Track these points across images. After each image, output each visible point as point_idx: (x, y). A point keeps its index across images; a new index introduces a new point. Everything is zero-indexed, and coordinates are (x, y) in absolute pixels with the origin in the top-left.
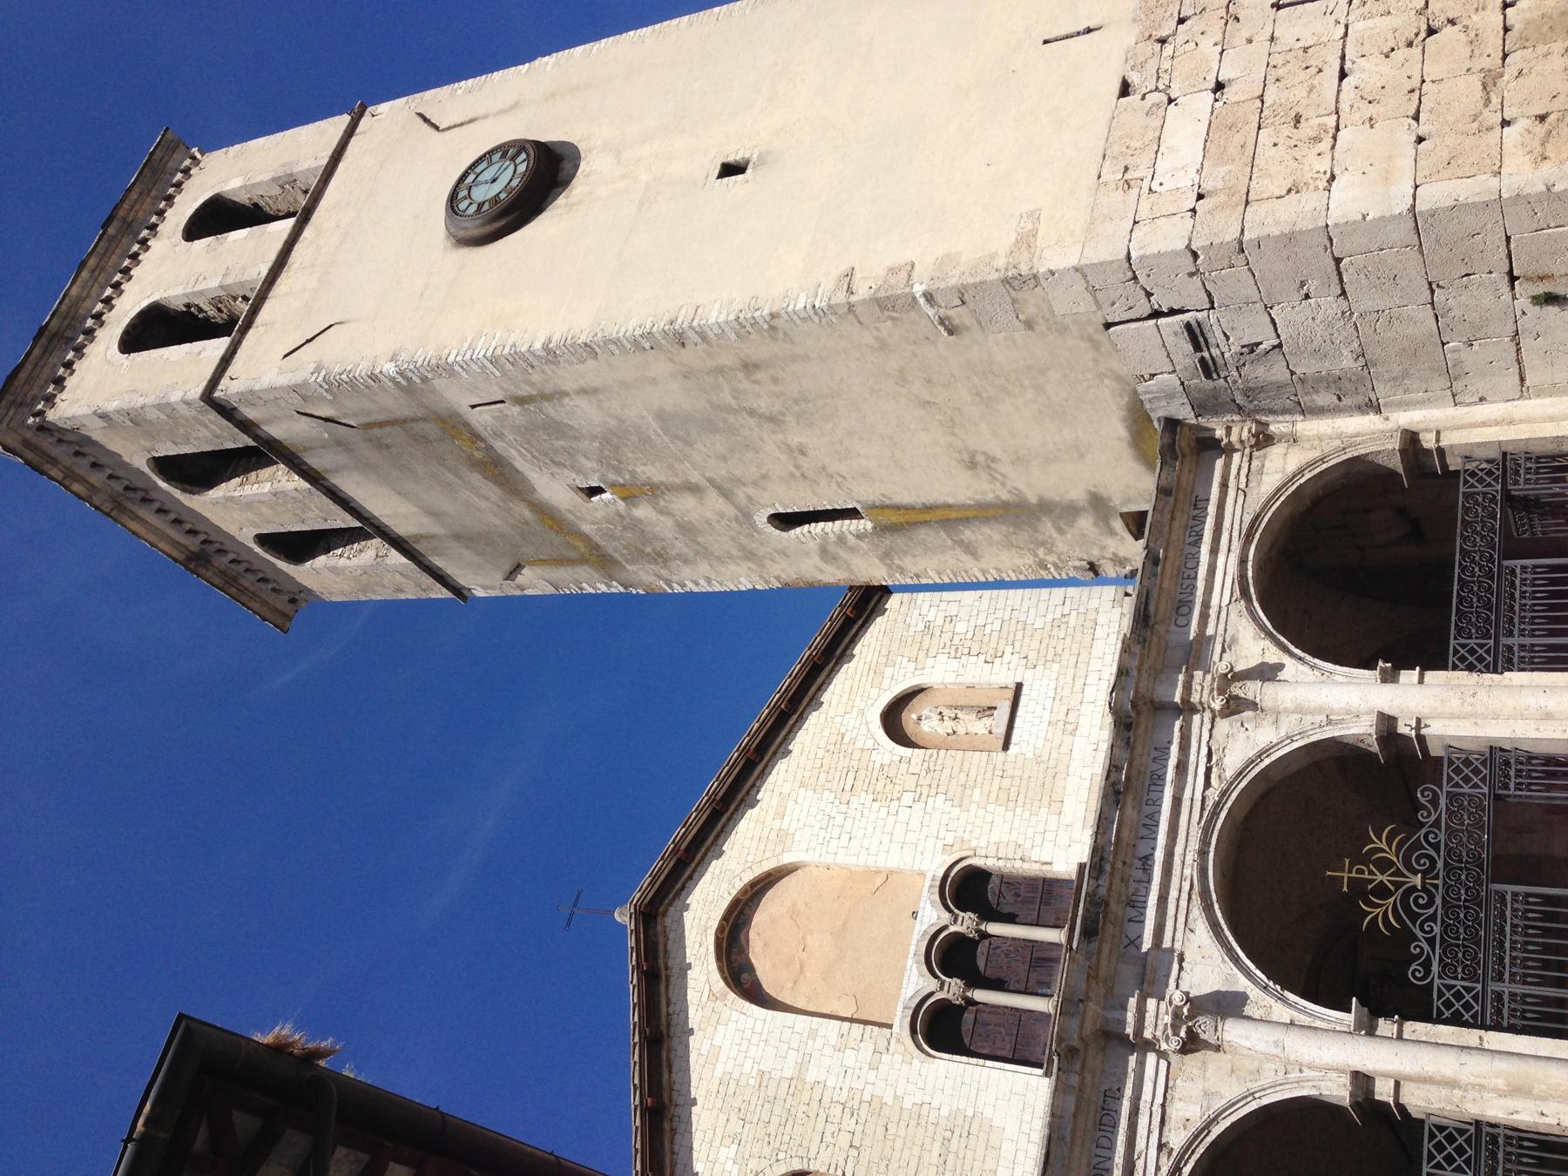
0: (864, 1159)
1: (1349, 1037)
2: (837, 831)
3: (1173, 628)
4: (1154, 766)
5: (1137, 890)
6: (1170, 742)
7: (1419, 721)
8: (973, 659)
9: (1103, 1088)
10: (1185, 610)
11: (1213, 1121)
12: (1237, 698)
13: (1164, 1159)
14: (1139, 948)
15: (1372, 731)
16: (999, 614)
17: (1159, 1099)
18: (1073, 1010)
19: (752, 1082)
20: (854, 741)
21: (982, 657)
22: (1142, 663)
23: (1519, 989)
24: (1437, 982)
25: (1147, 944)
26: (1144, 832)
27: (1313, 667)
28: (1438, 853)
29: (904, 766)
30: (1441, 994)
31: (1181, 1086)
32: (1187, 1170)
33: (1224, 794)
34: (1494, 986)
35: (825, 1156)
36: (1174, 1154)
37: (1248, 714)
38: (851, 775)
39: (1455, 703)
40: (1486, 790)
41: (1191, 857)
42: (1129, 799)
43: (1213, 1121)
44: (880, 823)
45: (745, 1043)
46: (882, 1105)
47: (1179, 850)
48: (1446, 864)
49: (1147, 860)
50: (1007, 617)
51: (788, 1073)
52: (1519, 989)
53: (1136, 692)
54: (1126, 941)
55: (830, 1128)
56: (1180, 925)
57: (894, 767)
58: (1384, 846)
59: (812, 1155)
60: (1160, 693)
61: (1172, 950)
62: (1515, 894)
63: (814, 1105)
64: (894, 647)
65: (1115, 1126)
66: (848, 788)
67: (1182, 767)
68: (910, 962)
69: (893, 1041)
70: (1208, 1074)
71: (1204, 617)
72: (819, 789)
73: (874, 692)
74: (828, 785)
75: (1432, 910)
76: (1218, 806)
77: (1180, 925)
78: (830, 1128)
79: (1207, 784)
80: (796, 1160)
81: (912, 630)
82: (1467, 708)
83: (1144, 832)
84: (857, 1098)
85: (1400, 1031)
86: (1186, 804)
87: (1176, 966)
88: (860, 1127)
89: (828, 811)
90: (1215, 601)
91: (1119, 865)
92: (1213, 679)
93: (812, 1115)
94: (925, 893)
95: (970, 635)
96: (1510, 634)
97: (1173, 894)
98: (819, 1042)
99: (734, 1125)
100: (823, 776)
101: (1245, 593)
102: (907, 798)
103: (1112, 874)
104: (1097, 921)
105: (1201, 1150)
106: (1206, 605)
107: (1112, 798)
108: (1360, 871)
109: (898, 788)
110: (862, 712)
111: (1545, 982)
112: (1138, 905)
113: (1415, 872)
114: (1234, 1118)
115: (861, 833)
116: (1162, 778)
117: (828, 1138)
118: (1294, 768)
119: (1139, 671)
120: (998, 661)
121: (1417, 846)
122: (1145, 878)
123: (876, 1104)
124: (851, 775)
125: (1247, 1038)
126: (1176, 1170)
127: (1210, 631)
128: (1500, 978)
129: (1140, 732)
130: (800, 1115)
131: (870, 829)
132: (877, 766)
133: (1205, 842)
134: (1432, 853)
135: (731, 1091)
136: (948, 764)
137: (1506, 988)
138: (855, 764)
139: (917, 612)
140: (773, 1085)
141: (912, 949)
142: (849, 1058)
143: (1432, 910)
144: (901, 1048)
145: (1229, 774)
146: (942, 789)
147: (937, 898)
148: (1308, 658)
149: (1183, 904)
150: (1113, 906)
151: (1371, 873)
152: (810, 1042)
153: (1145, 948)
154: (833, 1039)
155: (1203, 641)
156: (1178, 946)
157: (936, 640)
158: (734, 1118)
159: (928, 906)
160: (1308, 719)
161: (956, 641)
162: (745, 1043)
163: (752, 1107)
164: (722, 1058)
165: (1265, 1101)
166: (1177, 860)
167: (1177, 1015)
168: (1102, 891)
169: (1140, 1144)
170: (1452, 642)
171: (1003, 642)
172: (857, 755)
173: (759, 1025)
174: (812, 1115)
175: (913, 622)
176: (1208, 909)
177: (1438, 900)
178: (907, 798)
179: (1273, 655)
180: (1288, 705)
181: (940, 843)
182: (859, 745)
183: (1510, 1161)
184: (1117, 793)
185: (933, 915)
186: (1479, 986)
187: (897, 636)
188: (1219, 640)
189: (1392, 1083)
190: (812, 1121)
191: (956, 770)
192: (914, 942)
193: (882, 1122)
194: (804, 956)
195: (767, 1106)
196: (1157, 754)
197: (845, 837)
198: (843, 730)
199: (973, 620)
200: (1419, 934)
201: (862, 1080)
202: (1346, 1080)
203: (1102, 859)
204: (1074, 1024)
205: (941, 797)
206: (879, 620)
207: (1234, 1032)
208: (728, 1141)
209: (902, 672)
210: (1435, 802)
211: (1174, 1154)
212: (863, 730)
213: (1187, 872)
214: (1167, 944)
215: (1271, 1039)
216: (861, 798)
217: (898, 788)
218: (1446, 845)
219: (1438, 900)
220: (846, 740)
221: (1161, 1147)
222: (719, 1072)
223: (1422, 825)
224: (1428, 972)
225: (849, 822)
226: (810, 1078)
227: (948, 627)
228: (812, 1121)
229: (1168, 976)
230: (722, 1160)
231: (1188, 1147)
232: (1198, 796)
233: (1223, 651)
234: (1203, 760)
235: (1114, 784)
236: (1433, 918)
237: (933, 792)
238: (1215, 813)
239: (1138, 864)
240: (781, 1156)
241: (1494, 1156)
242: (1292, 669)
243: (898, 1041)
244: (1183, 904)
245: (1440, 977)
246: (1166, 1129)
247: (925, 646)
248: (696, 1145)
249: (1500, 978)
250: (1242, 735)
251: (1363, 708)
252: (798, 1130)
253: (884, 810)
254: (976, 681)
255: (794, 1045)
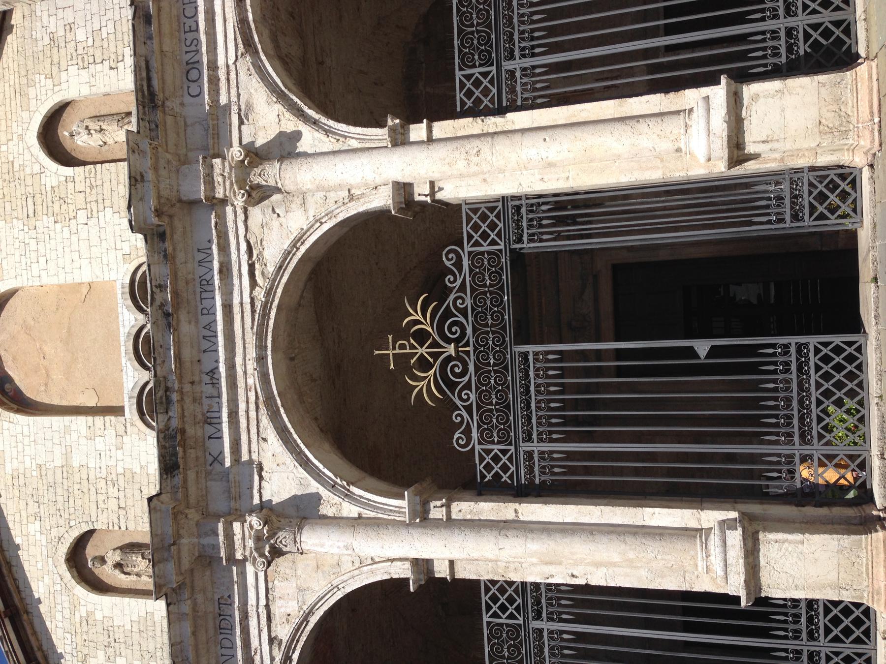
0: (131, 516)
1: (404, 531)
2: (34, 255)
3: (188, 99)
4: (202, 271)
5: (210, 406)
6: (210, 241)
7: (432, 184)
8: (99, 67)
9: (216, 597)
10: (194, 74)
11: (310, 612)
12: (259, 186)
13: (276, 651)
14: (222, 464)
15: (390, 202)
16: (110, 14)
17: (263, 602)
18: (166, 555)
19: (34, 473)
20: (23, 167)
21: (106, 63)
22: (157, 159)
23: (547, 447)
24: (478, 448)
25: (228, 463)
26: (205, 345)
27: (328, 132)
28: (466, 318)
29: (71, 185)
30: (482, 459)
31: (280, 587)
32: (295, 656)
33: (270, 292)
34: (525, 447)
35: (103, 518)
36: (284, 645)
37: (276, 197)
38: (30, 200)
39: (461, 165)
40: (502, 247)
41: (251, 365)
42: (183, 316)
43: (310, 612)
44: (67, 243)
45: (20, 445)
46: (133, 474)
47: (239, 360)
48: (475, 330)
49: (213, 372)
50: (117, 18)
51: (58, 463)
52: (547, 447)
53: (159, 197)
54: (211, 459)
55: (101, 498)
56: (254, 437)
57: (62, 188)
58: (419, 317)
59: (94, 519)
60: (187, 193)
61: (251, 461)
62: (536, 354)
63: (85, 482)
64: (30, 64)
65: (232, 628)
66: (31, 215)
67: (225, 270)
68: (124, 360)
69: (128, 425)
70: (299, 572)
71: (214, 81)
72: (8, 220)
73: (25, 115)
74: (15, 214)
75: (466, 378)
76: (266, 306)
77: (254, 437)
78: (101, 498)
79: (253, 284)
80: (83, 524)
81: (40, 44)
82: (474, 169)
83: (205, 345)
84: (114, 472)
85: (449, 513)
86: (237, 309)
87: (256, 478)
88: (122, 494)
89: (21, 237)
90: (221, 62)
91: (187, 388)
92: (231, 167)
93: (85, 490)
94: (120, 301)
95: (90, 42)
96: (511, 57)
97: (242, 406)
98: (74, 435)
99: (33, 508)
100: (8, 205)
101: (249, 44)
102: (82, 216)
103: (181, 400)
104: (175, 454)
105: (304, 638)
106: (213, 66)
107: (162, 322)
108: (402, 347)
109: (72, 207)
110: (21, 137)
111: (569, 437)
112: (212, 421)
113: (448, 341)
114: (326, 607)
115: (54, 256)
116: (210, 283)
117: (101, 505)
118: (334, 239)
119: (156, 169)
120: (121, 65)
121: (448, 314)
122: (216, 394)
123: (128, 475)
124: (30, 200)
125: (322, 546)
126: (287, 658)
127: (223, 100)
128: (529, 439)
129: (178, 236)
130: (77, 492)
131: (60, 249)
132: (49, 189)
133: (261, 346)
134: (461, 319)
135: (22, 483)
136: (106, 178)
137: (535, 447)
138: (30, 189)
139: (39, 24)
140: (50, 473)
141: (123, 349)
142: (100, 444)
143: (466, 378)
144: (135, 430)
145: (271, 269)
146: (108, 203)
147: (129, 302)
148: (323, 120)
149: (253, 414)
150: (190, 431)
151: (412, 347)
152: (67, 436)
153: (228, 463)
154: (84, 431)
155: (220, 113)
156: (255, 457)
157: (63, 51)
158: (31, 503)
159: (125, 311)
160: (332, 196)
161: (80, 51)
162: (20, 445)
163: (41, 492)
164: (8, 460)
165: (349, 590)
166: (239, 370)
167: (258, 538)
168: (175, 423)
169: (255, 643)
170: (458, 74)
171: (120, 44)
172: (29, 181)
173: (26, 429)
174: (85, 490)
175: (39, 36)
176: (274, 416)
177: (471, 367)
178: (82, 216)
179: (291, 124)
180: (309, 186)
181: (120, 254)
182: (28, 171)
183: (551, 605)
184: (167, 315)
185: (129, 319)
186: (512, 448)
187: (29, 53)
188: (234, 108)
189: (447, 563)
190: (87, 496)
191: (114, 182)
192: (123, 343)
193: (137, 486)
194: (46, 363)
195: (51, 490)
196: (201, 256)
197: (42, 260)
198: (11, 159)
199: (89, 23)
200: (458, 403)
201: (113, 459)
202: (407, 565)
203: (167, 389)
204: (170, 567)
205: (109, 211)
206: (9, 38)
207: (310, 542)
208: (32, 519)
209: (43, 90)
210: (459, 265)
211: (284, 645)
212: (27, 156)
213: (250, 381)
214: (245, 457)
215: (341, 544)
216: (45, 221)
217: (72, 207)
218: (473, 310)
219: (471, 367)
220: (16, 168)
221: (271, 641)
222: (9, 470)
223: (451, 289)
224: (469, 439)
225: (41, 246)
226: (76, 464)
227: (70, 36)
228: (87, 496)
229: (251, 488)
230: (32, 533)
231: (294, 638)
232: (247, 300)
233: (241, 123)
234: (244, 257)
235: (162, 306)
236: (468, 386)
237: (101, 207)
238: (265, 315)
239: (207, 379)
240: (72, 523)
241: (538, 602)
242: (311, 140)
243: (132, 425)
244: (253, 414)
245: (480, 443)
246: (273, 625)
247: (56, 60)
248: (11, 525)
249: (529, 439)
250: (275, 223)
251: (378, 181)
252: (79, 503)
253: (66, 230)
254: (107, 90)
255: (57, 441)
